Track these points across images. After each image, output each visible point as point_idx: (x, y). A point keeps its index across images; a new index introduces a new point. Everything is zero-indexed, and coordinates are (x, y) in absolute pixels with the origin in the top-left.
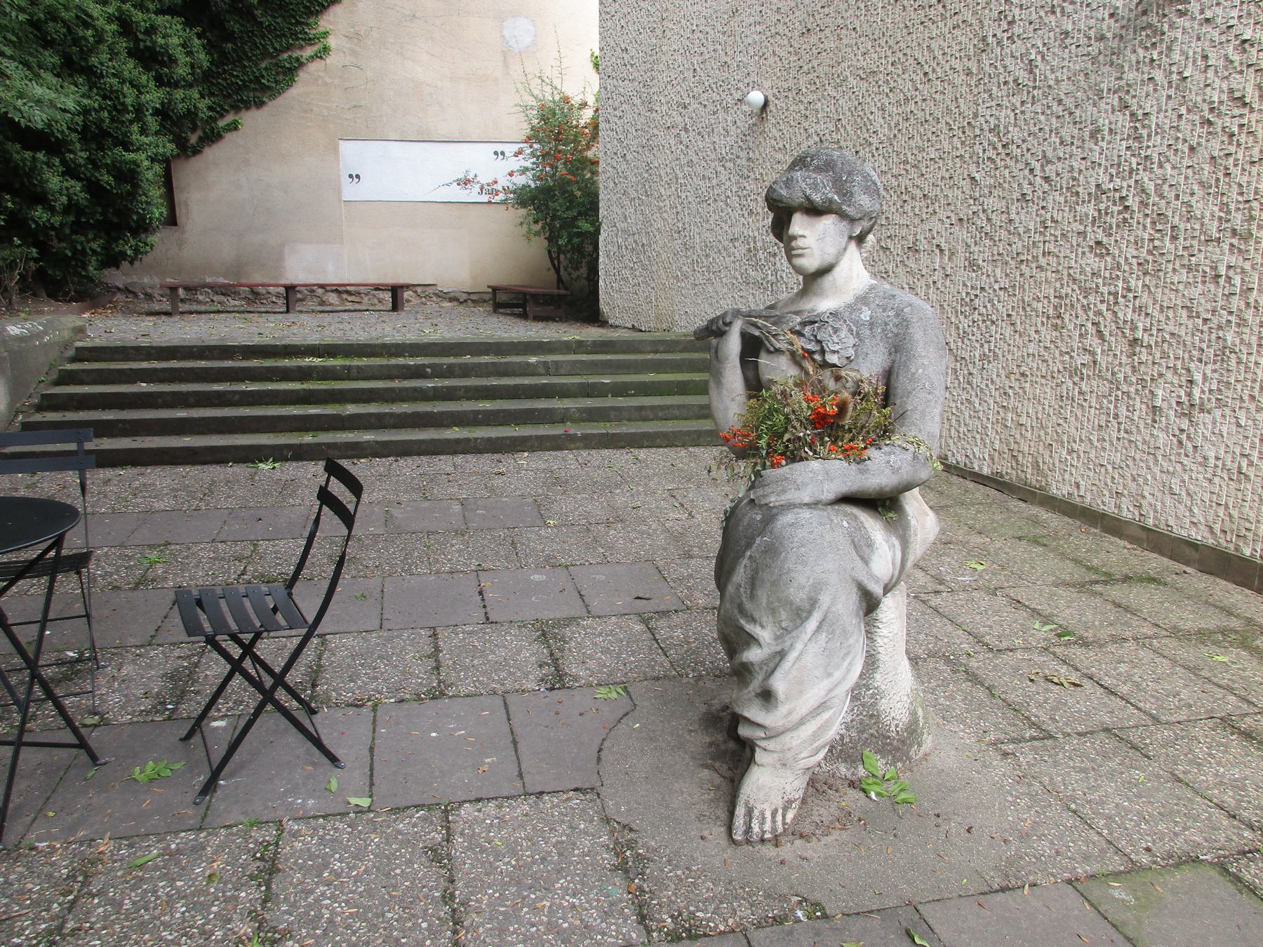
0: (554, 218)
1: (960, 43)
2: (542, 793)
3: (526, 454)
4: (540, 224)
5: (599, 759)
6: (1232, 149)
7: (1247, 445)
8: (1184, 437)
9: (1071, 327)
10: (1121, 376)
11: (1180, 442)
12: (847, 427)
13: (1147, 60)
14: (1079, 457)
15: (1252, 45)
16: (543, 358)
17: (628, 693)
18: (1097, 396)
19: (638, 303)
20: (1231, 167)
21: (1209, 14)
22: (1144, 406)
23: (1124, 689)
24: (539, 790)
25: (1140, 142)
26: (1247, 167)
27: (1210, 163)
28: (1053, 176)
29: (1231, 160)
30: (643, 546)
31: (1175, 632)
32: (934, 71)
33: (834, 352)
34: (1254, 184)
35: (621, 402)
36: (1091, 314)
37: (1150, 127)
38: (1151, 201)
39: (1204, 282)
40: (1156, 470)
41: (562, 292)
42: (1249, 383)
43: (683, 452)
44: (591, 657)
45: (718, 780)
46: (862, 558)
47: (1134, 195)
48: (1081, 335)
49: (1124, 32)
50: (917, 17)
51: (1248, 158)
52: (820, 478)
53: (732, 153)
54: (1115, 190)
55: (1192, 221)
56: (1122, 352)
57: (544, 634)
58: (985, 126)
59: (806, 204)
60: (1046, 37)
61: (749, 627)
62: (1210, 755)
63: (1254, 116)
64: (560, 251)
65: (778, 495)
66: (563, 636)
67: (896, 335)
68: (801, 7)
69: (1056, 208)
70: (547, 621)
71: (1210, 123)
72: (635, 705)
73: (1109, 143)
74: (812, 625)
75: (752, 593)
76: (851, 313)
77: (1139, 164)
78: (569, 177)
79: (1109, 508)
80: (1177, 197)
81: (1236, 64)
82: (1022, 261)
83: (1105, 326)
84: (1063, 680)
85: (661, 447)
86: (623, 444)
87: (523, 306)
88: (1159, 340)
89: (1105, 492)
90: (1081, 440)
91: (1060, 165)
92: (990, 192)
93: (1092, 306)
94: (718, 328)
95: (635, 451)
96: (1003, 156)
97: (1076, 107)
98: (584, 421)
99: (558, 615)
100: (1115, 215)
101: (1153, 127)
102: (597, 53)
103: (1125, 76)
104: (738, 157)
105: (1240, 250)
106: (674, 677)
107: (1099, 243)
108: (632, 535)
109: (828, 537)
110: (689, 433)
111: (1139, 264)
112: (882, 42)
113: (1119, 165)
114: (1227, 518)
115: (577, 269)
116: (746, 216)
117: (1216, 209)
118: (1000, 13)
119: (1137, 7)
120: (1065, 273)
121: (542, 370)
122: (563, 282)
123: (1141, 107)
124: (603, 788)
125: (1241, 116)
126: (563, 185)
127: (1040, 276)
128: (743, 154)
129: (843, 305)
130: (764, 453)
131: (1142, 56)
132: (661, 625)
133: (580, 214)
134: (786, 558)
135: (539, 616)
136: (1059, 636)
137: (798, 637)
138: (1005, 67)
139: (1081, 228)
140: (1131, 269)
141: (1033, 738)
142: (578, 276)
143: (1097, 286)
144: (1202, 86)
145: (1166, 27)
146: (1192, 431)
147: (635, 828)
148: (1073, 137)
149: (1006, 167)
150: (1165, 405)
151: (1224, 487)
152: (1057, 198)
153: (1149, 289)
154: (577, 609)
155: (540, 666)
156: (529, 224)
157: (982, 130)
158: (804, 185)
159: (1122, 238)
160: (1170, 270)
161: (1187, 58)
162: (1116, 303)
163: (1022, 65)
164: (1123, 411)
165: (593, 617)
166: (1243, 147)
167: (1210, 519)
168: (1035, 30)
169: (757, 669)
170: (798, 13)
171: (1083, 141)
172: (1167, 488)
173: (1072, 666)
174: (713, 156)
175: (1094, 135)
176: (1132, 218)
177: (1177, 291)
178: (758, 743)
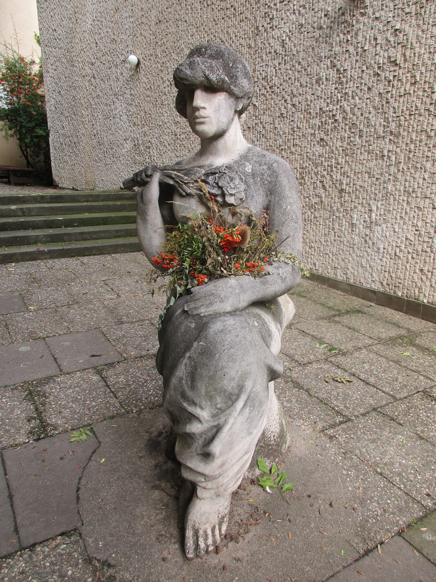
0: (21, 127)
1: (245, 30)
2: (34, 545)
3: (13, 264)
4: (13, 130)
5: (78, 498)
6: (390, 89)
7: (399, 242)
8: (368, 238)
9: (309, 184)
10: (335, 208)
11: (366, 241)
12: (245, 250)
13: (345, 41)
14: (315, 250)
15: (400, 32)
16: (20, 206)
17: (94, 433)
18: (323, 219)
19: (74, 175)
20: (390, 98)
21: (377, 15)
22: (347, 224)
23: (372, 380)
24: (32, 542)
25: (342, 85)
26: (397, 98)
27: (379, 97)
28: (297, 103)
29: (389, 95)
30: (92, 318)
31: (380, 340)
32: (231, 46)
33: (232, 195)
34: (401, 107)
35: (70, 230)
36: (319, 177)
37: (347, 77)
38: (348, 117)
39: (376, 159)
40: (354, 255)
41: (30, 169)
42: (400, 211)
43: (109, 257)
44: (65, 407)
45: (166, 499)
46: (267, 345)
47: (340, 114)
48: (314, 188)
49: (332, 25)
50: (220, 15)
51: (398, 94)
52: (237, 291)
53: (121, 91)
54: (330, 111)
55: (370, 127)
56: (335, 196)
57: (30, 393)
58: (260, 77)
59: (205, 82)
60: (291, 27)
61: (191, 409)
62: (428, 416)
63: (401, 71)
64: (27, 147)
65: (207, 307)
66: (44, 393)
67: (270, 182)
68: (155, 8)
69: (299, 121)
70: (32, 382)
71: (378, 75)
72: (100, 442)
73: (326, 86)
74: (240, 404)
75: (192, 384)
76: (238, 167)
77: (341, 97)
78: (28, 103)
79: (331, 275)
80: (362, 114)
81: (392, 43)
82: (282, 149)
83: (326, 183)
84: (343, 380)
85: (96, 255)
86: (73, 254)
87: (8, 177)
88: (354, 189)
89: (329, 267)
90: (316, 241)
91: (300, 97)
92: (264, 113)
93: (319, 173)
94: (142, 179)
95: (81, 258)
96: (270, 93)
97: (308, 66)
98: (49, 242)
99: (40, 375)
100: (330, 124)
101: (349, 77)
102: (38, 35)
103: (333, 49)
104: (125, 93)
105: (394, 142)
106: (123, 414)
107: (322, 139)
108: (85, 312)
109: (249, 338)
110: (111, 246)
111: (343, 150)
112: (202, 29)
113: (331, 98)
114: (390, 278)
115: (38, 156)
116: (132, 126)
117: (382, 121)
118: (265, 13)
119: (339, 11)
120: (305, 155)
121: (20, 214)
122: (30, 164)
123: (342, 66)
124: (84, 527)
125: (394, 71)
126: (25, 108)
127: (292, 157)
128: (128, 92)
129: (232, 161)
130: (187, 271)
131: (342, 38)
132: (110, 373)
133: (36, 125)
134: (220, 358)
135: (26, 378)
136: (330, 350)
137: (230, 414)
138: (269, 44)
139: (313, 131)
140: (339, 153)
141: (341, 423)
142: (39, 161)
143: (322, 162)
144: (374, 55)
145: (354, 23)
146: (372, 235)
147: (113, 562)
148: (307, 82)
149: (272, 99)
150: (358, 223)
151: (388, 263)
152: (299, 115)
153: (348, 163)
154: (52, 370)
155: (29, 421)
156: (6, 130)
157: (258, 78)
158: (203, 67)
159: (334, 136)
160: (359, 153)
161: (366, 40)
162: (332, 171)
163: (278, 43)
164: (337, 226)
165: (64, 374)
166: (395, 88)
167: (381, 278)
168: (285, 23)
169: (198, 437)
170: (153, 11)
171: (312, 85)
172: (360, 264)
173: (342, 369)
174: (111, 93)
175: (318, 81)
176: (339, 126)
177: (363, 164)
178: (199, 484)
